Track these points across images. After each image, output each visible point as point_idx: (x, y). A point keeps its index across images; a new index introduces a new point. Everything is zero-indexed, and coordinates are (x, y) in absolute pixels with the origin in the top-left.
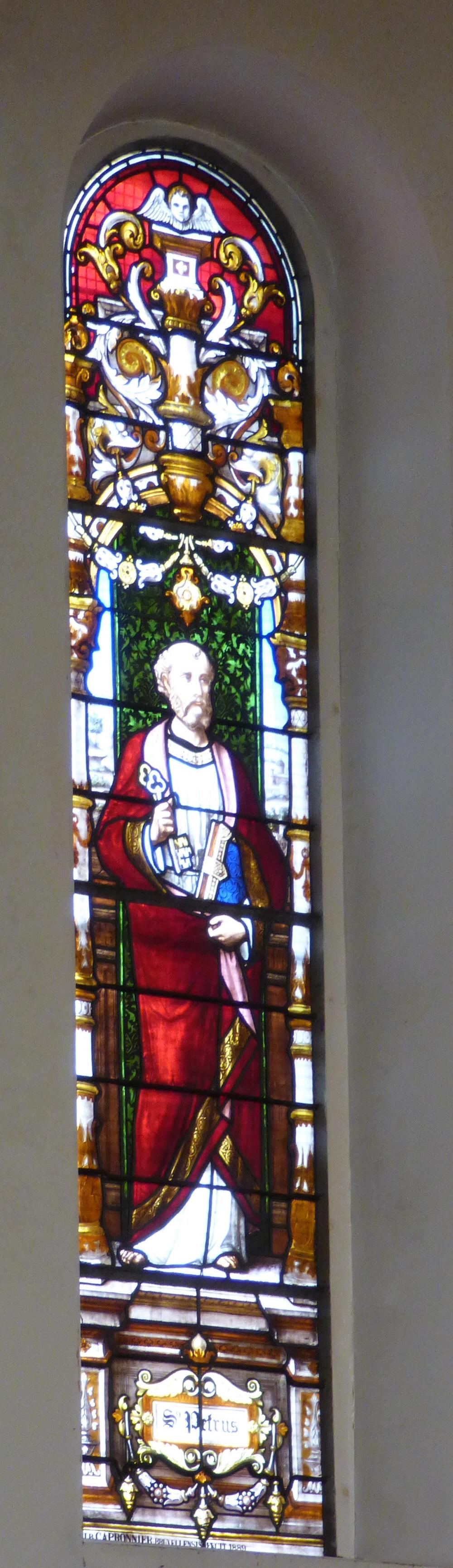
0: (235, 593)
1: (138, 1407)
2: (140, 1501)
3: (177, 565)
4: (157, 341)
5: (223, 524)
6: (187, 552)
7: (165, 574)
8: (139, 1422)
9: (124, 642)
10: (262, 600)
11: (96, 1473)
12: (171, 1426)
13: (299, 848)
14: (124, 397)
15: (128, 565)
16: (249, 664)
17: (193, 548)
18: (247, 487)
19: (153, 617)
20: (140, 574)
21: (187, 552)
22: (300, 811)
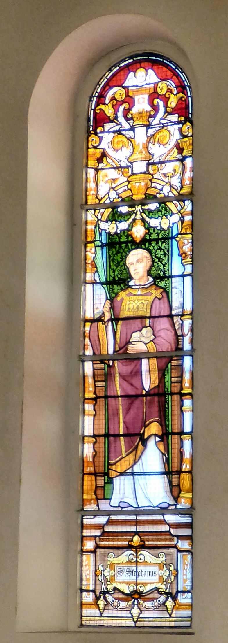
0: (160, 225)
1: (108, 569)
2: (107, 608)
3: (134, 220)
4: (130, 133)
5: (155, 197)
6: (138, 213)
7: (129, 226)
8: (108, 575)
9: (111, 257)
10: (173, 224)
11: (88, 596)
12: (121, 575)
13: (187, 323)
14: (164, 116)
15: (114, 225)
16: (167, 251)
17: (141, 211)
18: (166, 180)
19: (123, 243)
20: (118, 227)
21: (138, 213)
22: (188, 307)
